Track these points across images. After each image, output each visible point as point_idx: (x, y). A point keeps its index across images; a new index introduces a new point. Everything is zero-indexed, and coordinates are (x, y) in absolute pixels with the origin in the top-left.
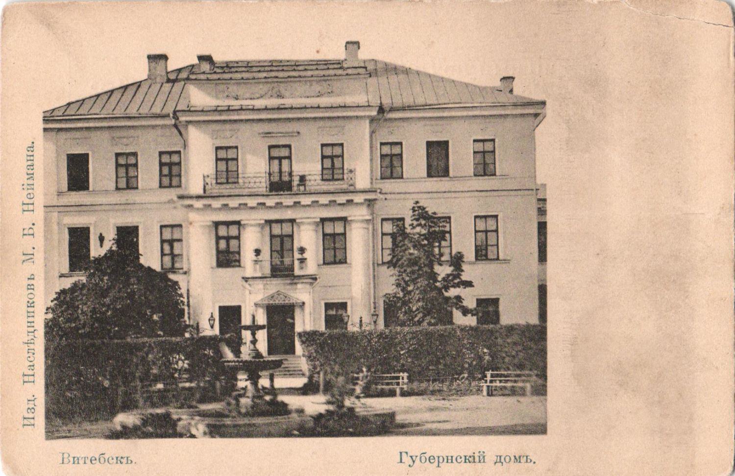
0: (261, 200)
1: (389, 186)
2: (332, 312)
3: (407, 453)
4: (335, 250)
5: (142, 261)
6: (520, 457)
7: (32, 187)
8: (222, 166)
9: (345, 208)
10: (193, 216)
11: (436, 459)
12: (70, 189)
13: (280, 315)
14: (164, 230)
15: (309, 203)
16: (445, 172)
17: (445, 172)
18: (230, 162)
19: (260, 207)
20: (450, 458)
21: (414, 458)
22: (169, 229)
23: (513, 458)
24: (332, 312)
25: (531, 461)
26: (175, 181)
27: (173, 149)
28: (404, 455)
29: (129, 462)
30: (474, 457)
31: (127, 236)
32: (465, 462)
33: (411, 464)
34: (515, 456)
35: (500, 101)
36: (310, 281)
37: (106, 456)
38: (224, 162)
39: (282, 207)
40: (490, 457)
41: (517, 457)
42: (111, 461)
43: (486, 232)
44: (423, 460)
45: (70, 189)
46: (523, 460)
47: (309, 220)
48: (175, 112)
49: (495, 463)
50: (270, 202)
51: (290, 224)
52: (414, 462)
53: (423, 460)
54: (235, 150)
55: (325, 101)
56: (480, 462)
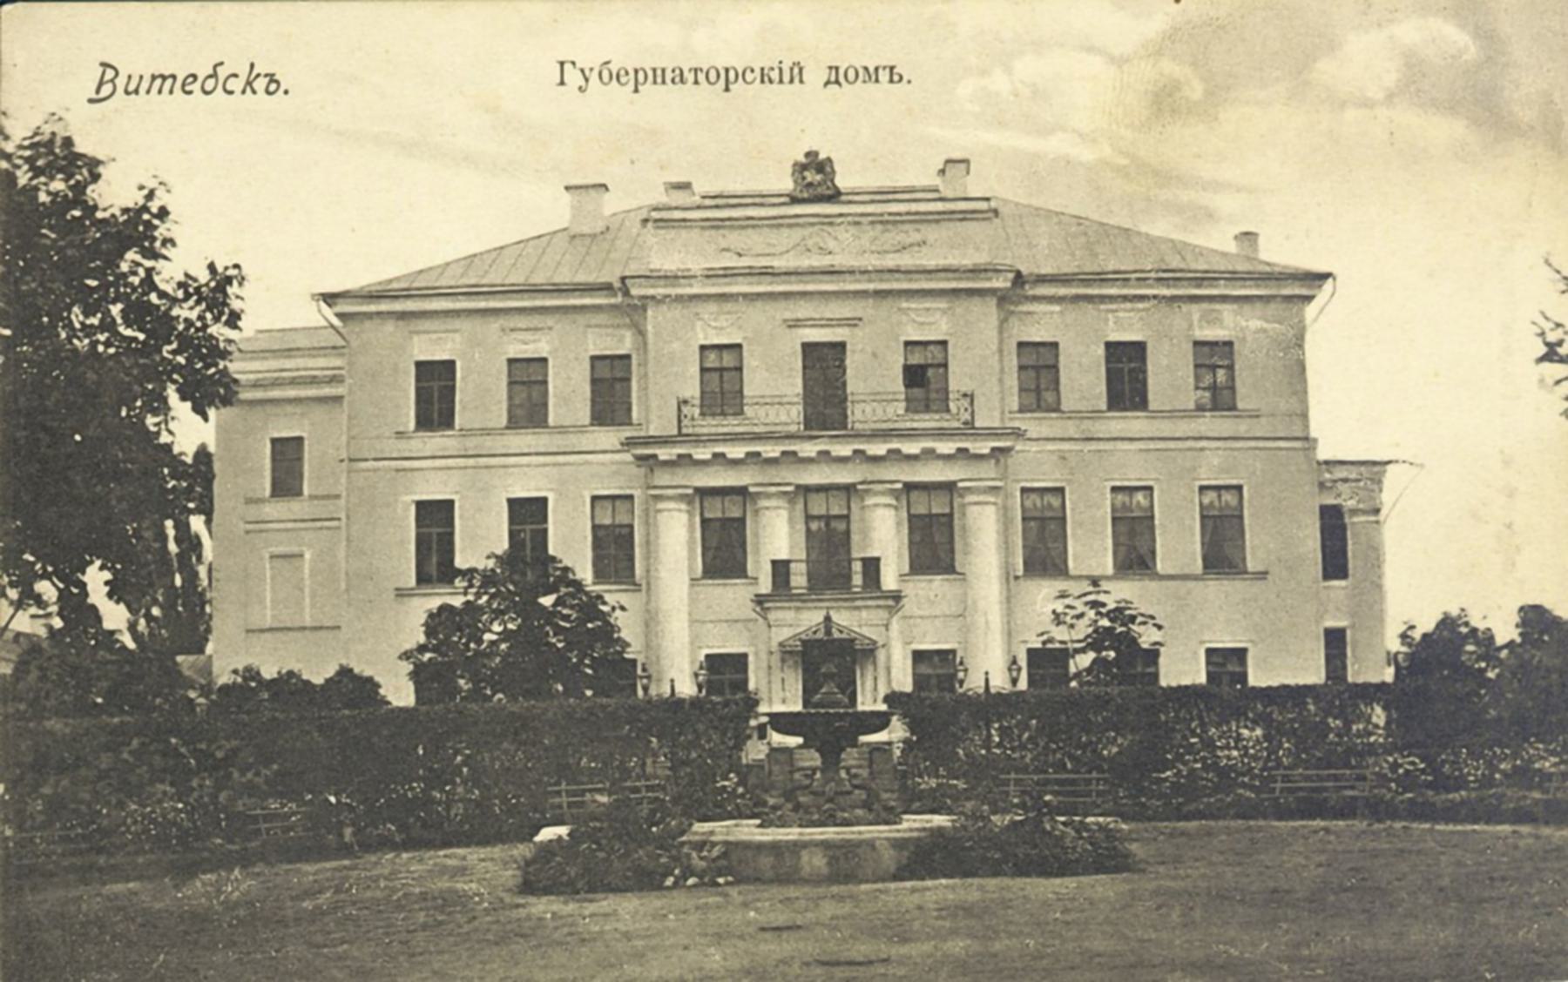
1: (1033, 425)
3: (573, 63)
4: (934, 547)
6: (877, 69)
8: (522, 394)
9: (918, 465)
12: (1111, 407)
13: (829, 662)
14: (598, 504)
16: (446, 421)
17: (446, 421)
22: (608, 504)
23: (861, 72)
27: (725, 341)
28: (568, 67)
30: (781, 70)
31: (528, 515)
33: (583, 83)
34: (866, 69)
35: (1194, 266)
36: (891, 602)
37: (614, 68)
39: (827, 463)
41: (872, 70)
42: (749, 76)
45: (1111, 407)
46: (884, 76)
48: (623, 279)
50: (808, 449)
51: (843, 495)
52: (587, 80)
54: (734, 354)
55: (906, 260)
56: (792, 81)
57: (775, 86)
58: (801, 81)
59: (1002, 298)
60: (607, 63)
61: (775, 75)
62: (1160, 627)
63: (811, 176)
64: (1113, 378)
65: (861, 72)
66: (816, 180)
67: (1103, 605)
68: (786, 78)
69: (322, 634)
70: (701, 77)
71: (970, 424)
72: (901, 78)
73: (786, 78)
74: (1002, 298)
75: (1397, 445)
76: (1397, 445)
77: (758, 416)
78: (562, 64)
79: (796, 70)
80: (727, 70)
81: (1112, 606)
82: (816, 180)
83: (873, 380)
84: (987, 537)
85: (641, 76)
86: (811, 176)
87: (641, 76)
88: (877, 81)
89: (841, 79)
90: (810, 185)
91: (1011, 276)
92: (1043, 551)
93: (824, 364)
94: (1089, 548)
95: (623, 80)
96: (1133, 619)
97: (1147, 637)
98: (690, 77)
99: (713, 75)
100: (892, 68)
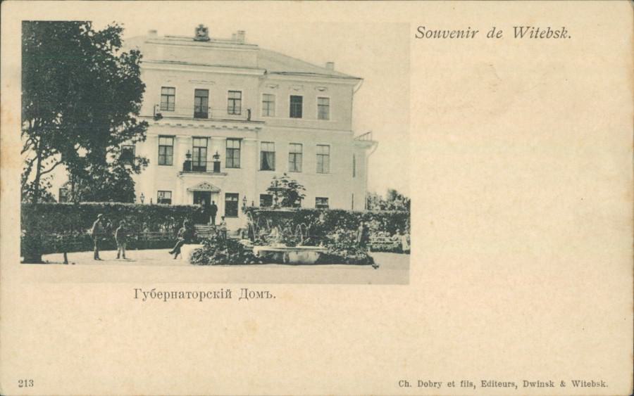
0: (191, 122)
2: (230, 199)
5: (80, 156)
6: (262, 292)
7: (229, 297)
10: (217, 132)
11: (164, 294)
15: (232, 127)
18: (236, 101)
19: (189, 127)
20: (174, 296)
21: (146, 294)
23: (256, 293)
24: (230, 199)
25: (271, 296)
26: (270, 112)
28: (138, 291)
29: (269, 296)
32: (215, 297)
38: (166, 97)
39: (201, 128)
40: (444, 385)
41: (260, 293)
43: (200, 148)
44: (153, 296)
46: (265, 295)
47: (219, 138)
49: (240, 299)
50: (230, 125)
53: (153, 296)
54: (239, 94)
56: (227, 297)
57: (220, 299)
58: (230, 297)
59: (261, 78)
60: (154, 290)
61: (220, 295)
62: (304, 189)
63: (201, 33)
64: (300, 108)
65: (256, 293)
66: (202, 35)
67: (287, 182)
68: (225, 295)
69: (55, 261)
70: (191, 296)
71: (249, 120)
72: (271, 296)
73: (225, 295)
74: (261, 78)
75: (432, 223)
76: (432, 223)
77: (179, 112)
78: (136, 290)
79: (228, 293)
80: (201, 293)
81: (290, 182)
82: (202, 35)
83: (218, 105)
84: (249, 157)
85: (167, 294)
86: (201, 33)
87: (167, 294)
88: (262, 297)
89: (248, 296)
90: (200, 36)
91: (264, 71)
92: (266, 163)
93: (202, 95)
94: (282, 166)
95: (160, 297)
96: (296, 186)
97: (300, 192)
98: (186, 295)
99: (195, 294)
100: (268, 292)
